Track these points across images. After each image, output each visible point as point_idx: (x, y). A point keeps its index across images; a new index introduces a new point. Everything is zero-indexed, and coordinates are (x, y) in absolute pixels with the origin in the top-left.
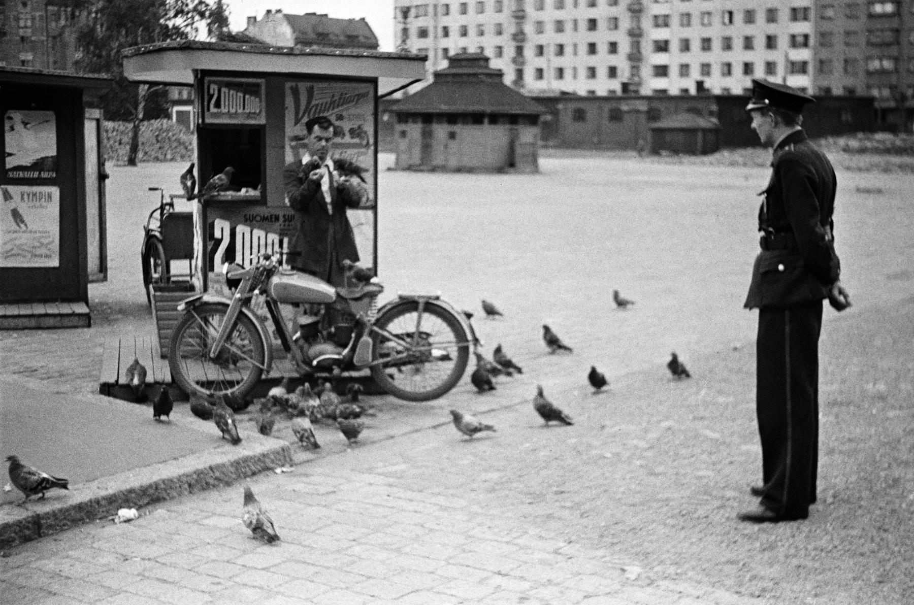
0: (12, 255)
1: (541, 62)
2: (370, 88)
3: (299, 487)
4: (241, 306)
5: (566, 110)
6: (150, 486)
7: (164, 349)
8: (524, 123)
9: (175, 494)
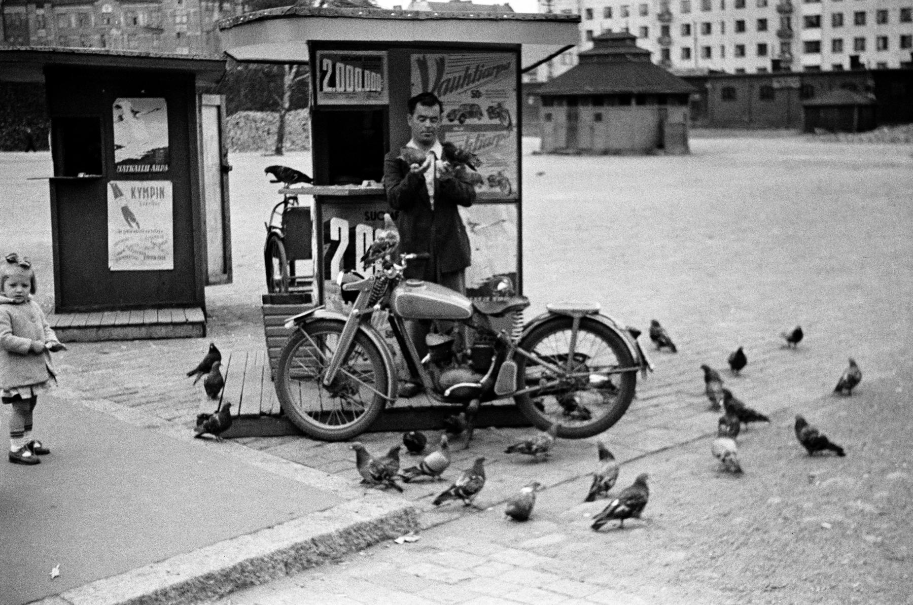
0: (123, 257)
1: (688, 42)
2: (510, 58)
3: (425, 569)
4: (360, 324)
5: (715, 90)
6: (235, 568)
7: (274, 370)
8: (673, 104)
9: (267, 577)
